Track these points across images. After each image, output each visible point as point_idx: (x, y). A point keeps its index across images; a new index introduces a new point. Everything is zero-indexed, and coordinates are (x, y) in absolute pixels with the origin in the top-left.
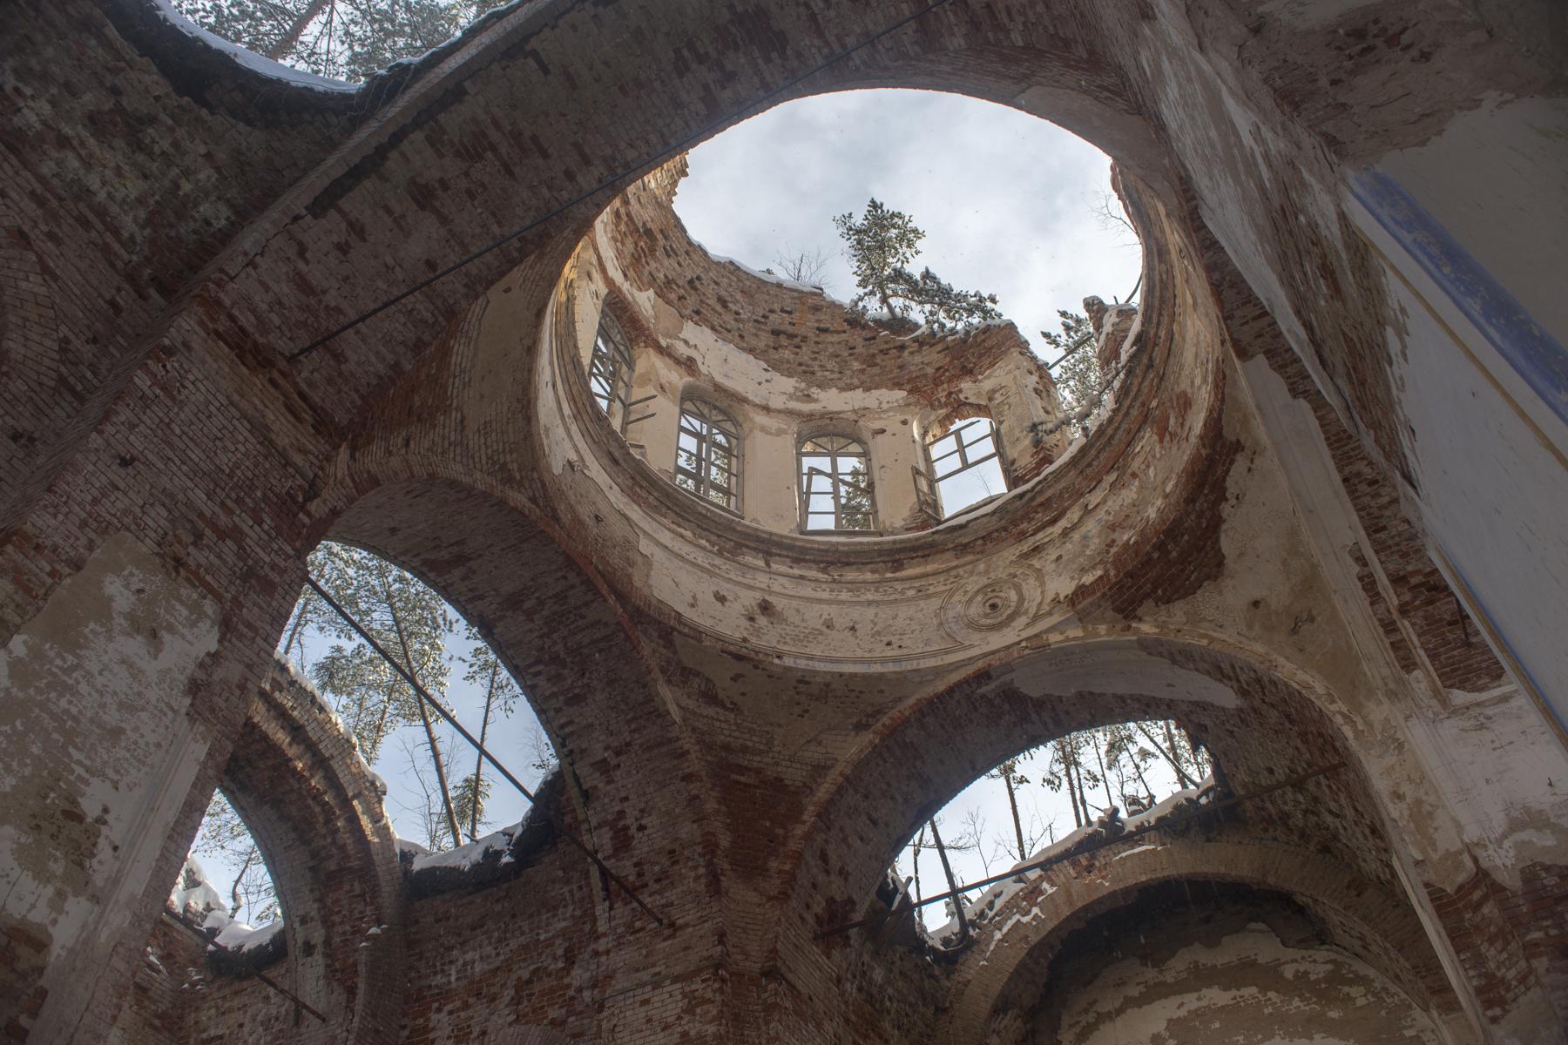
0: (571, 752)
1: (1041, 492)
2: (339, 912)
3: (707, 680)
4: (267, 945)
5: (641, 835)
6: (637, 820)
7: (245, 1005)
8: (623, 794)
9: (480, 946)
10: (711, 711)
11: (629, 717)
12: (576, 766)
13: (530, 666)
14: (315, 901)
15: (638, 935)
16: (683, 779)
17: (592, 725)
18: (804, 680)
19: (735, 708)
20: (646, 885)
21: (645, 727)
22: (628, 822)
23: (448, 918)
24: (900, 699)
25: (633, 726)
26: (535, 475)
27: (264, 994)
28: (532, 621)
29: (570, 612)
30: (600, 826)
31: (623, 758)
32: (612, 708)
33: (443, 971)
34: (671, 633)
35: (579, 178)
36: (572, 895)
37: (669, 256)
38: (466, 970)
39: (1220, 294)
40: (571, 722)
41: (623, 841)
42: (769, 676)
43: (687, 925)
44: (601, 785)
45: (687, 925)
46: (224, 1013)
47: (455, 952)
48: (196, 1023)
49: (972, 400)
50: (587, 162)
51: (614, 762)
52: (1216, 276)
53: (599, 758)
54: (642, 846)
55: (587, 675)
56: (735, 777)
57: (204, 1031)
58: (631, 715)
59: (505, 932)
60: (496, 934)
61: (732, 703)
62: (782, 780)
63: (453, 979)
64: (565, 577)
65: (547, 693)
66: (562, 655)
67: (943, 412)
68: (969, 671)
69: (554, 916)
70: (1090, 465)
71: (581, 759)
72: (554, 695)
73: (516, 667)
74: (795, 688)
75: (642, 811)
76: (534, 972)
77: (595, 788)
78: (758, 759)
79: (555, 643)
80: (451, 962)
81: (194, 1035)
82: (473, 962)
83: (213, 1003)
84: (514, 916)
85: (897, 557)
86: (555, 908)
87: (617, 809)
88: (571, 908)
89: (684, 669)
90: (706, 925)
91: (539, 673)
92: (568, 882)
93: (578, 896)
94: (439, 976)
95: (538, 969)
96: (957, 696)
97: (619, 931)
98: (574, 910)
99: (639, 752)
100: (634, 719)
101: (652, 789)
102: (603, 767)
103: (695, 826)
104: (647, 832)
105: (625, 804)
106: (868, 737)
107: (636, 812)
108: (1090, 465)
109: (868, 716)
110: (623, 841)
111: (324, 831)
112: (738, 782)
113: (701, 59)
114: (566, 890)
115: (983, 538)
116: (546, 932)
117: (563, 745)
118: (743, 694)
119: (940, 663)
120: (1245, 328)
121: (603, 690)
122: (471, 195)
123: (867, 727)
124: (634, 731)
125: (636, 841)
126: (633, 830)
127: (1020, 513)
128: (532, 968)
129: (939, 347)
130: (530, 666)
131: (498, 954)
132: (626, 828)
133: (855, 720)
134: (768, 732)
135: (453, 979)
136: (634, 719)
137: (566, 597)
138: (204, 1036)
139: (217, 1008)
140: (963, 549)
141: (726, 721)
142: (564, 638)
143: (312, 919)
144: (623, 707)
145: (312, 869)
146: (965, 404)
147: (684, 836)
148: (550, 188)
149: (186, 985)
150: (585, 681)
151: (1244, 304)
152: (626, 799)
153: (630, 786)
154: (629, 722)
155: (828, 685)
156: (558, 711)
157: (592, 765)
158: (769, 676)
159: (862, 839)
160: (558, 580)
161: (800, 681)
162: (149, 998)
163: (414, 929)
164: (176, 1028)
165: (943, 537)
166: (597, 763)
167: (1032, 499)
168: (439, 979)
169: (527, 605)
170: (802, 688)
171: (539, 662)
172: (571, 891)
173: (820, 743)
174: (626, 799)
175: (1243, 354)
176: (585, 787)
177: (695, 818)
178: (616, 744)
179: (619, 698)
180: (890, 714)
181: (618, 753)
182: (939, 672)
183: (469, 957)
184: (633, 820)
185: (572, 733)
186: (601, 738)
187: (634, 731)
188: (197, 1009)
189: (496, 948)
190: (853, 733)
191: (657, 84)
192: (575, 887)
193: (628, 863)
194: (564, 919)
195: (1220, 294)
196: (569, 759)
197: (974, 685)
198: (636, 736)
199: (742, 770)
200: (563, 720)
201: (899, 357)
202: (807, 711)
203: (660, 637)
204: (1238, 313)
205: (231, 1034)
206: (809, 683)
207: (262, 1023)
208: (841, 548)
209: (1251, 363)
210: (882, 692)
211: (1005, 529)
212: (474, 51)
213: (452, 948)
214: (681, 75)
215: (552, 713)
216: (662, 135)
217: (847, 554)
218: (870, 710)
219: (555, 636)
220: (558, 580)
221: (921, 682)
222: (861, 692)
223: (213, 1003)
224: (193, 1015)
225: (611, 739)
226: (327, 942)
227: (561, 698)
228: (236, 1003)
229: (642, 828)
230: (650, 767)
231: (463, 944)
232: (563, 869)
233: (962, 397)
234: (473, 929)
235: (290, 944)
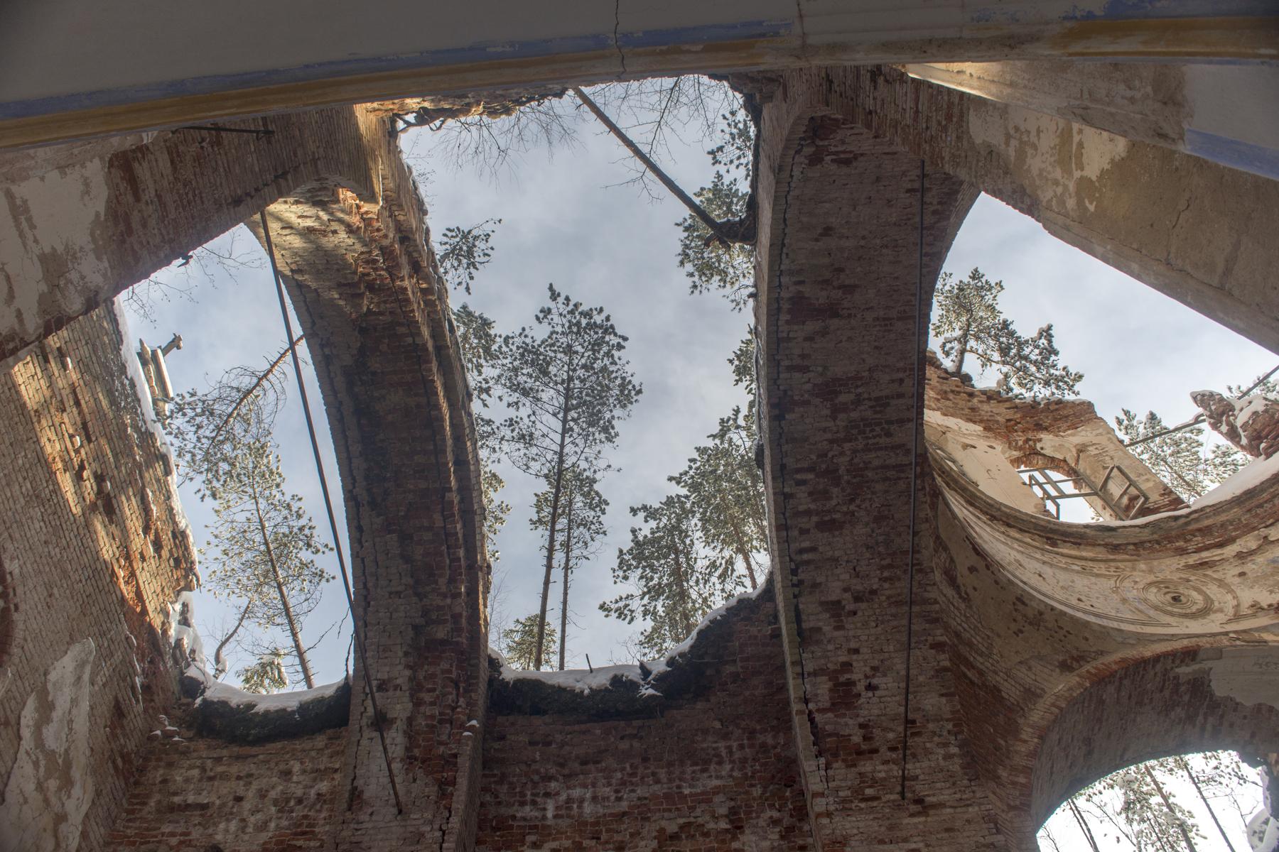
0: (801, 582)
1: (1197, 520)
2: (433, 690)
3: (952, 560)
4: (293, 712)
5: (870, 694)
6: (866, 677)
7: (250, 775)
8: (853, 645)
9: (594, 785)
11: (884, 563)
12: (802, 599)
13: (798, 471)
14: (408, 667)
15: (870, 803)
16: (933, 646)
17: (836, 560)
18: (1021, 600)
19: (966, 599)
20: (876, 751)
21: (899, 579)
22: (855, 677)
23: (549, 744)
24: (1102, 653)
25: (886, 574)
27: (282, 767)
28: (835, 419)
29: (880, 424)
30: (815, 674)
31: (863, 605)
32: (868, 547)
33: (534, 803)
36: (731, 752)
38: (570, 808)
40: (813, 549)
41: (844, 696)
43: (941, 805)
44: (826, 629)
45: (941, 805)
46: (211, 779)
47: (553, 784)
48: (165, 781)
49: (1048, 452)
51: (850, 606)
53: (834, 598)
54: (869, 707)
55: (858, 502)
56: (963, 668)
57: (175, 794)
58: (888, 561)
59: (633, 775)
60: (619, 775)
61: (966, 593)
62: (999, 691)
63: (550, 814)
64: (901, 381)
65: (801, 508)
66: (842, 471)
67: (1016, 454)
68: (1178, 645)
69: (703, 771)
70: (1260, 506)
71: (811, 593)
72: (808, 513)
73: (783, 467)
74: (1014, 604)
75: (875, 669)
76: (682, 827)
77: (819, 630)
78: (981, 660)
79: (842, 454)
80: (547, 795)
81: (157, 797)
82: (582, 801)
83: (198, 763)
84: (645, 760)
85: (1051, 536)
86: (707, 762)
87: (843, 659)
88: (728, 767)
90: (970, 809)
91: (803, 482)
92: (726, 736)
93: (737, 755)
94: (528, 808)
95: (689, 824)
96: (1159, 667)
97: (841, 794)
98: (732, 770)
99: (885, 604)
100: (890, 566)
101: (891, 648)
102: (835, 609)
103: (944, 700)
104: (878, 693)
105: (855, 657)
106: (1073, 679)
107: (868, 669)
108: (1260, 506)
109: (1073, 658)
110: (844, 696)
111: (444, 589)
114: (721, 745)
115: (1135, 544)
116: (691, 786)
117: (794, 572)
118: (975, 589)
119: (1140, 631)
121: (867, 524)
123: (1070, 669)
124: (885, 580)
125: (862, 700)
126: (860, 687)
127: (1173, 533)
128: (682, 821)
129: (1008, 405)
130: (798, 471)
131: (619, 799)
132: (851, 683)
133: (1061, 658)
135: (550, 814)
136: (890, 566)
137: (888, 404)
138: (177, 799)
139: (203, 769)
140: (1115, 548)
142: (855, 451)
143: (397, 687)
144: (881, 549)
145: (415, 627)
146: (1038, 453)
147: (929, 707)
149: (158, 732)
150: (852, 507)
152: (856, 651)
153: (864, 638)
154: (882, 568)
155: (1041, 613)
156: (803, 532)
157: (822, 603)
160: (893, 381)
161: (1018, 599)
162: (122, 727)
163: (497, 745)
164: (132, 780)
165: (1093, 533)
166: (827, 603)
167: (1187, 524)
168: (527, 811)
169: (843, 398)
170: (1020, 607)
171: (811, 469)
172: (729, 748)
174: (856, 651)
176: (804, 625)
177: (944, 691)
178: (859, 588)
179: (881, 539)
180: (1094, 664)
181: (858, 599)
182: (1142, 639)
183: (576, 793)
184: (861, 676)
185: (808, 562)
186: (842, 577)
187: (885, 580)
188: (170, 765)
189: (617, 791)
190: (1058, 670)
192: (735, 745)
193: (851, 722)
194: (717, 777)
196: (796, 590)
197: (1178, 662)
198: (886, 585)
199: (971, 666)
200: (806, 544)
201: (969, 401)
202: (1021, 632)
205: (224, 805)
206: (1026, 605)
207: (275, 802)
208: (1003, 509)
210: (1087, 639)
211: (1158, 542)
213: (550, 778)
215: (795, 533)
217: (1008, 515)
218: (1075, 653)
219: (847, 446)
220: (893, 381)
221: (1122, 643)
223: (198, 763)
224: (161, 771)
225: (854, 581)
226: (410, 720)
227: (815, 519)
228: (234, 769)
229: (870, 687)
230: (895, 623)
231: (568, 777)
232: (721, 720)
233: (1039, 446)
234: (584, 763)
235: (355, 711)
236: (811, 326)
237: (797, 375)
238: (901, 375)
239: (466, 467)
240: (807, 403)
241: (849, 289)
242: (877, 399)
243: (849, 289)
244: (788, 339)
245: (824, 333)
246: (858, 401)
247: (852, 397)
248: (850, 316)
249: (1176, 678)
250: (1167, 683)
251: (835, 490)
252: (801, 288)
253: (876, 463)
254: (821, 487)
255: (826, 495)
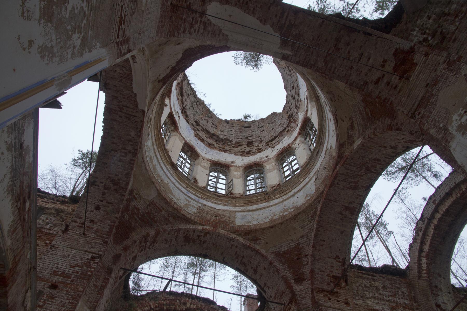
3: (348, 129)
10: (356, 126)
19: (351, 118)
26: (313, 204)
34: (341, 144)
35: (236, 245)
37: (291, 109)
39: (141, 129)
42: (337, 110)
50: (232, 245)
52: (139, 134)
79: (362, 173)
89: (348, 137)
112: (371, 115)
113: (201, 241)
118: (346, 117)
120: (140, 116)
122: (251, 263)
134: (352, 107)
137: (344, 179)
141: (356, 120)
148: (241, 249)
151: (137, 122)
158: (337, 110)
159: (369, 59)
160: (339, 185)
173: (345, 90)
175: (143, 112)
191: (211, 242)
195: (141, 129)
203: (343, 147)
204: (139, 121)
209: (143, 109)
212: (262, 205)
214: (206, 241)
216: (218, 237)
219: (359, 174)
220: (339, 185)
222: (322, 83)
236: (352, 206)
237: (361, 194)
238: (337, 185)
239: (456, 242)
240: (362, 186)
241: (341, 213)
242: (345, 181)
243: (341, 213)
244: (358, 203)
245: (350, 203)
246: (350, 183)
247: (351, 184)
248: (343, 205)
249: (292, 50)
250: (296, 49)
251: (369, 166)
252: (351, 217)
253: (355, 168)
254: (372, 168)
255: (372, 166)
